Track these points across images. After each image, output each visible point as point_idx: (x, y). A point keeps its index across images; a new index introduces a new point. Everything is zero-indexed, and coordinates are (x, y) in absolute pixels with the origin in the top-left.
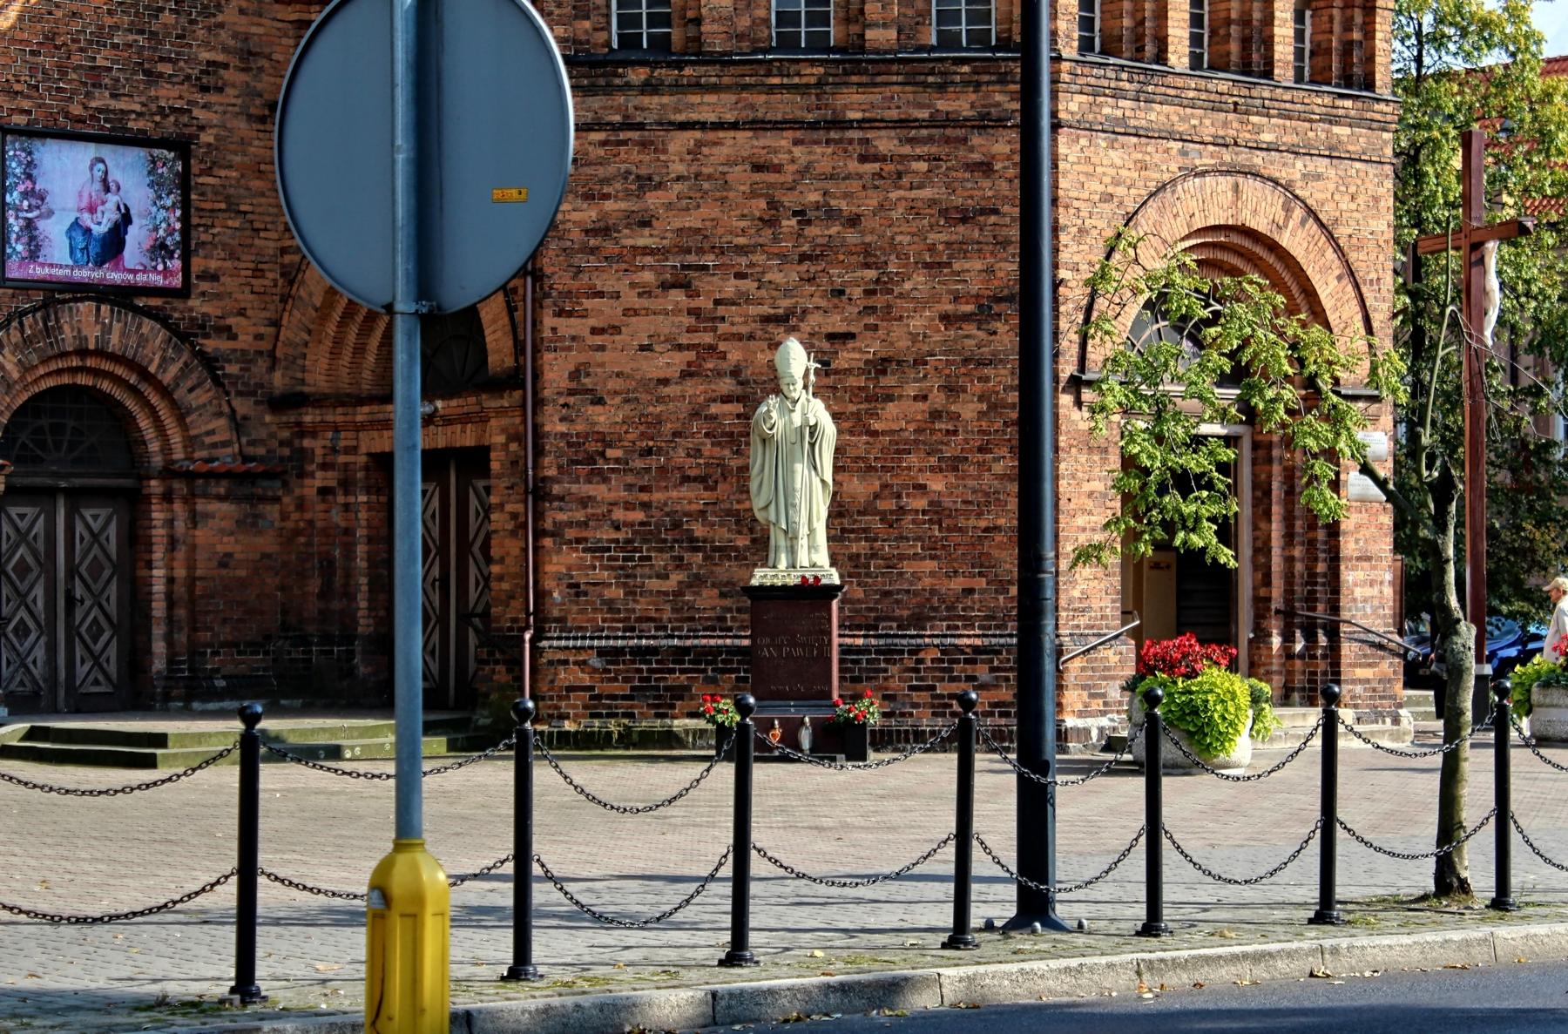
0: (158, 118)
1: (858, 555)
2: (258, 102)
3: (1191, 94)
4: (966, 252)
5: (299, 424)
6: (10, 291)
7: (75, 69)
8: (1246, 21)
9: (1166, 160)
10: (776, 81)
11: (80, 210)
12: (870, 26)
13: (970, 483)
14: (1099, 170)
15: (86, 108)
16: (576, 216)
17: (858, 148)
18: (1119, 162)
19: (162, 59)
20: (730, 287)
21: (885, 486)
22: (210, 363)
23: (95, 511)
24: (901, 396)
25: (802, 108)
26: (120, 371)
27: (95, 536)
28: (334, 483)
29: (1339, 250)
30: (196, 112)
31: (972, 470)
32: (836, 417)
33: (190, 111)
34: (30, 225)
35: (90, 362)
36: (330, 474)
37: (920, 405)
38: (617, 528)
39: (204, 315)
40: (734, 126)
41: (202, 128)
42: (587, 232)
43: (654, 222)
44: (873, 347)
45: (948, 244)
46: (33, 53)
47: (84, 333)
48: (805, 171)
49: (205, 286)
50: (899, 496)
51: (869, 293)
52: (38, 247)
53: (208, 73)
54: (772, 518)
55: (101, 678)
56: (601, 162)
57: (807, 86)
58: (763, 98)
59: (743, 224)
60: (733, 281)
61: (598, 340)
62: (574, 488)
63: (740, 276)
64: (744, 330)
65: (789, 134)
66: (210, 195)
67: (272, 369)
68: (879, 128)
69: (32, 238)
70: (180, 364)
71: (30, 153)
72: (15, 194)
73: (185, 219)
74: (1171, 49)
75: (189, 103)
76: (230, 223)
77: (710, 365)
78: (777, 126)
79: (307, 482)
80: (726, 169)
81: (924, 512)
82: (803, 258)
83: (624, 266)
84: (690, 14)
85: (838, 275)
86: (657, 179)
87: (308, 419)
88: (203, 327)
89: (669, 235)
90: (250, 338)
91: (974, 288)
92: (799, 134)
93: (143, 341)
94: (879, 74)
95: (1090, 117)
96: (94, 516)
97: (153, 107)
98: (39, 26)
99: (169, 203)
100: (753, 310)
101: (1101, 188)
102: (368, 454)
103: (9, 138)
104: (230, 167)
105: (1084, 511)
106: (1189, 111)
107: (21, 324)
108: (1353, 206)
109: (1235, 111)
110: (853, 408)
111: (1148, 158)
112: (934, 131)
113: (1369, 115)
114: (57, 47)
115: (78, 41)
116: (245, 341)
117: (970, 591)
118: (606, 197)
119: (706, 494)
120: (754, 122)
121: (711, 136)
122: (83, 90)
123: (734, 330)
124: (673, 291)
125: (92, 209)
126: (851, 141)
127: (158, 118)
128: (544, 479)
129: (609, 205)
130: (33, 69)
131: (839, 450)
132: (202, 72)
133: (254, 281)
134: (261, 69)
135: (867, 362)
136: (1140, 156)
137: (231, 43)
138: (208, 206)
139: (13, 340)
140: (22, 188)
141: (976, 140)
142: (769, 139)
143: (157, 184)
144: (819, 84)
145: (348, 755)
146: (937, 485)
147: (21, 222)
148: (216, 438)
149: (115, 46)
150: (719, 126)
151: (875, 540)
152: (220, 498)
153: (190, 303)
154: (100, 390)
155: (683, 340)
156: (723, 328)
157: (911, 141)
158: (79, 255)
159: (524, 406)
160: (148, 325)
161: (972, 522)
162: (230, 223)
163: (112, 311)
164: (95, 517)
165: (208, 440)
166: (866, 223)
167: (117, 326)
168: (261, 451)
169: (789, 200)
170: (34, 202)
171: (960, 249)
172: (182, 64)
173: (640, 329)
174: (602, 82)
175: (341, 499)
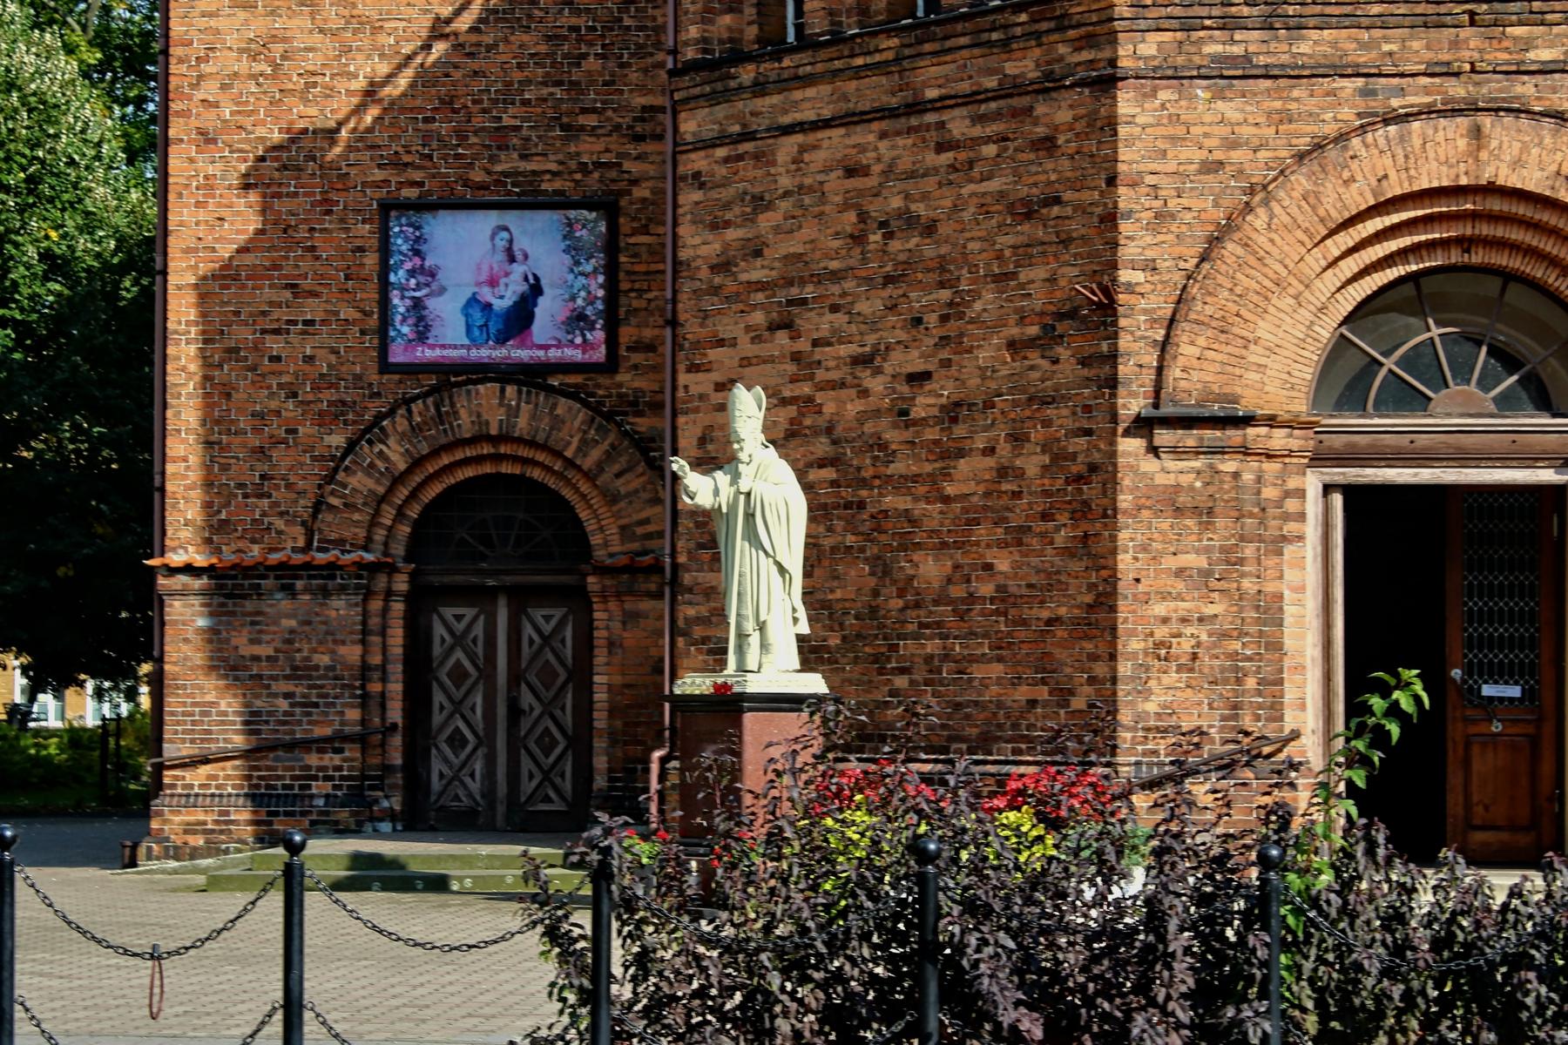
0: (578, 176)
1: (932, 657)
4: (1032, 256)
6: (397, 377)
7: (475, 133)
9: (1340, 104)
10: (859, 61)
11: (478, 284)
13: (1035, 561)
14: (1195, 130)
15: (489, 173)
16: (704, 251)
17: (933, 133)
18: (1236, 116)
19: (584, 111)
21: (957, 567)
23: (545, 612)
25: (886, 93)
27: (546, 639)
30: (627, 165)
31: (1035, 543)
33: (620, 165)
34: (417, 304)
39: (636, 390)
41: (635, 182)
43: (766, 251)
44: (944, 390)
46: (426, 120)
47: (485, 417)
49: (637, 358)
50: (968, 581)
51: (944, 319)
52: (427, 327)
53: (643, 120)
55: (552, 795)
57: (886, 62)
58: (854, 84)
59: (836, 244)
60: (829, 317)
63: (835, 309)
64: (834, 375)
65: (875, 126)
66: (644, 257)
68: (952, 107)
69: (421, 319)
70: (605, 446)
71: (418, 228)
72: (401, 273)
73: (612, 287)
75: (619, 155)
83: (741, 306)
85: (918, 300)
88: (635, 404)
89: (777, 264)
91: (1038, 305)
92: (884, 125)
93: (557, 423)
94: (946, 38)
95: (1180, 60)
96: (545, 617)
97: (573, 164)
98: (433, 91)
99: (588, 268)
100: (844, 350)
101: (1199, 155)
103: (393, 214)
105: (1165, 596)
106: (1377, 33)
107: (410, 411)
109: (1472, 23)
110: (928, 468)
111: (1293, 106)
112: (1002, 103)
114: (455, 111)
115: (480, 102)
117: (1033, 703)
121: (811, 138)
122: (486, 154)
125: (493, 282)
126: (928, 127)
127: (578, 176)
130: (426, 139)
132: (635, 119)
136: (1278, 104)
138: (642, 268)
139: (400, 429)
140: (408, 266)
143: (575, 250)
144: (898, 60)
145: (455, 887)
147: (408, 302)
151: (947, 637)
154: (531, 479)
155: (787, 393)
156: (820, 375)
158: (476, 332)
160: (563, 406)
163: (520, 392)
164: (547, 618)
165: (640, 531)
166: (944, 229)
170: (422, 279)
171: (1026, 253)
172: (610, 113)
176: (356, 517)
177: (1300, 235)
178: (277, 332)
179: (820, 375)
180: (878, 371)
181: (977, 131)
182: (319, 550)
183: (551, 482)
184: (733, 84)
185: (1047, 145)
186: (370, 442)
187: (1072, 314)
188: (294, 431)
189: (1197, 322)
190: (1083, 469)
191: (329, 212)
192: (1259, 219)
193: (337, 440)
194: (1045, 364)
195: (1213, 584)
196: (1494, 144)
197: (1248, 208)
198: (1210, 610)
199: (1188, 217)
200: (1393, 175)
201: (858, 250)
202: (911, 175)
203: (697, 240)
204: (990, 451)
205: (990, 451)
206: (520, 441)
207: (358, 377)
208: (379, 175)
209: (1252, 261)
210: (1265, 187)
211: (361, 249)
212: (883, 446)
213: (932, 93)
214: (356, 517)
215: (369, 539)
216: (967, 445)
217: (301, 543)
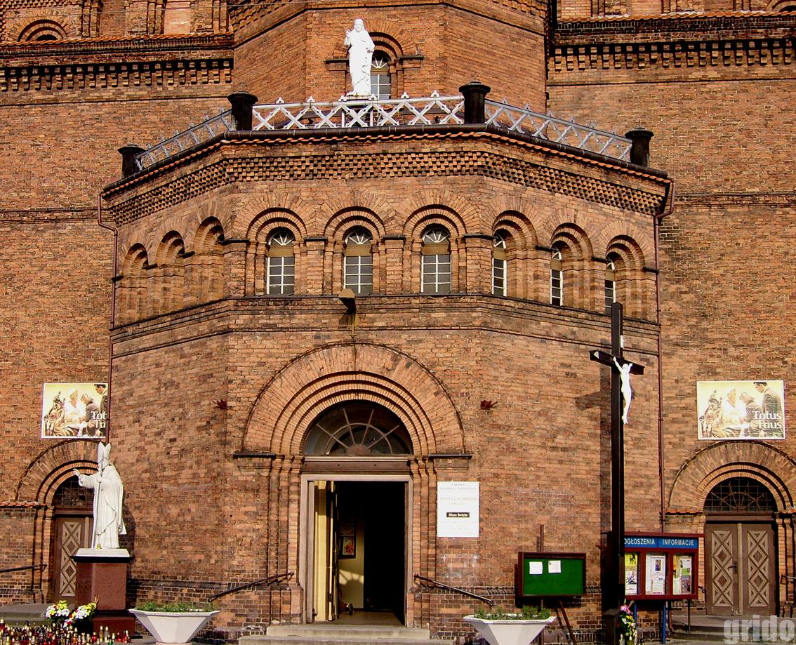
3: (320, 307)
9: (306, 342)
51: (180, 419)
59: (152, 391)
64: (151, 439)
105: (242, 521)
113: (457, 305)
166: (181, 386)
176: (33, 489)
177: (292, 389)
178: (9, 422)
179: (147, 439)
180: (162, 438)
181: (191, 351)
182: (20, 501)
184: (127, 334)
185: (209, 355)
186: (39, 462)
188: (13, 458)
189: (255, 421)
191: (28, 380)
192: (277, 383)
193: (28, 461)
194: (207, 435)
195: (259, 518)
196: (361, 356)
197: (273, 379)
198: (258, 527)
199: (252, 382)
200: (325, 367)
202: (174, 367)
204: (191, 467)
205: (191, 467)
208: (46, 367)
209: (274, 398)
210: (279, 372)
212: (162, 465)
213: (180, 338)
214: (33, 489)
215: (38, 496)
217: (14, 498)
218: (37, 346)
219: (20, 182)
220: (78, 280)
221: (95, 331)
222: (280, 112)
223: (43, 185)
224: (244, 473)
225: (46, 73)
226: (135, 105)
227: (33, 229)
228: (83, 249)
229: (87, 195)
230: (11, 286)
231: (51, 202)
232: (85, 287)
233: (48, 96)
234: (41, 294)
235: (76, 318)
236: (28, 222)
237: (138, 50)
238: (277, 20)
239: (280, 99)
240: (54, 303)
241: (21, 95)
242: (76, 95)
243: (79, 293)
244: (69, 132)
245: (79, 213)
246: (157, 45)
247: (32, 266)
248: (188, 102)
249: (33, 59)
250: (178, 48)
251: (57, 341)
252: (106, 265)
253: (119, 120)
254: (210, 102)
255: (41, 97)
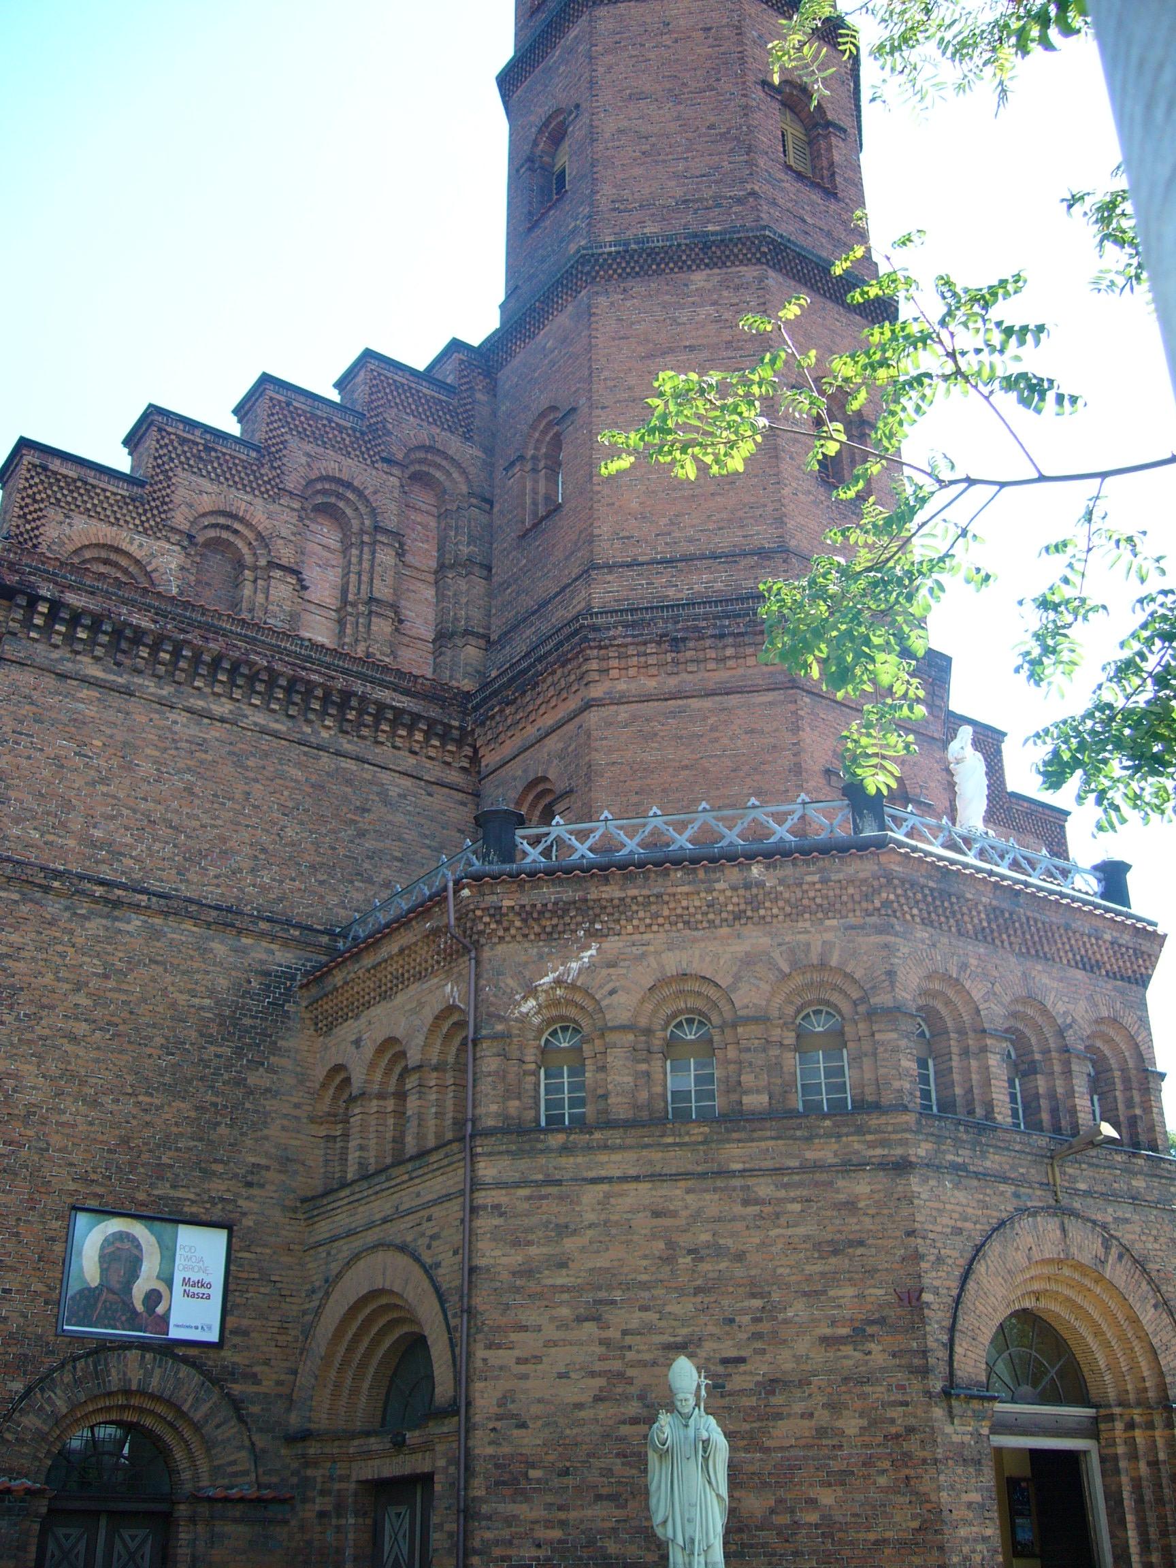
2: (292, 1196)
5: (304, 1456)
8: (1052, 1096)
10: (670, 1140)
12: (746, 1093)
16: (504, 1260)
18: (964, 1201)
19: (215, 1161)
20: (636, 1319)
21: (780, 1501)
22: (236, 1404)
23: (133, 1532)
24: (789, 1415)
26: (160, 1409)
27: (132, 1556)
28: (329, 1508)
29: (1150, 1281)
30: (240, 1202)
32: (728, 1435)
35: (134, 1401)
36: (326, 1499)
37: (806, 1423)
38: (539, 1546)
39: (234, 1363)
40: (636, 1179)
41: (244, 1214)
42: (514, 1274)
44: (760, 1368)
45: (823, 1274)
46: (110, 1151)
47: (130, 1375)
48: (696, 1216)
49: (236, 1340)
50: (792, 1512)
51: (757, 1320)
54: (670, 1534)
56: (528, 1214)
59: (645, 1263)
60: (638, 1314)
61: (522, 1369)
62: (501, 1507)
64: (647, 1357)
65: (682, 1184)
67: (289, 1410)
74: (996, 1110)
76: (262, 1290)
77: (619, 1390)
78: (675, 1177)
79: (308, 1506)
80: (630, 1216)
81: (817, 1526)
82: (698, 1291)
84: (600, 1092)
86: (572, 1227)
87: (312, 1451)
88: (233, 1374)
90: (271, 1383)
91: (847, 1313)
92: (690, 1183)
97: (206, 1197)
102: (359, 1482)
104: (265, 1246)
105: (966, 1523)
107: (74, 1368)
108: (1157, 1246)
110: (746, 1427)
116: (268, 1386)
118: (530, 1243)
119: (617, 1512)
120: (652, 1175)
121: (617, 1188)
123: (640, 1357)
124: (587, 1324)
128: (474, 1499)
129: (533, 1250)
131: (732, 1466)
133: (279, 1337)
134: (296, 1172)
135: (758, 1383)
137: (273, 1150)
138: (245, 1275)
141: (840, 1183)
142: (665, 1189)
146: (827, 1498)
148: (234, 1469)
149: (178, 1150)
150: (624, 1179)
152: (235, 1521)
153: (223, 1353)
156: (630, 1355)
157: (786, 1186)
159: (458, 1431)
160: (184, 1370)
161: (862, 1536)
162: (262, 1290)
164: (133, 1538)
165: (229, 1470)
166: (752, 1258)
167: (157, 1371)
168: (275, 1480)
169: (684, 1240)
171: (832, 1278)
173: (560, 1358)
174: (527, 1147)
175: (334, 1521)
176: (25, 1450)
181: (782, 1194)
183: (159, 1428)
186: (42, 1390)
187: (882, 1321)
190: (901, 1430)
193: (18, 1386)
201: (668, 1268)
203: (498, 1253)
206: (153, 1397)
207: (40, 1337)
208: (72, 1186)
211: (53, 1239)
214: (25, 1450)
216: (785, 1410)
218: (56, 1140)
219: (48, 813)
220: (148, 1025)
221: (174, 1129)
222: (705, 823)
223: (92, 831)
224: (960, 1429)
225: (124, 639)
226: (266, 742)
227: (67, 908)
228: (160, 969)
229: (174, 872)
230: (11, 1007)
231: (104, 867)
232: (159, 1040)
233: (112, 677)
234: (73, 1039)
235: (141, 1098)
236: (59, 894)
237: (297, 655)
238: (711, 686)
239: (655, 809)
240: (97, 1061)
241: (62, 659)
242: (164, 693)
243: (148, 1051)
244: (148, 751)
245: (162, 902)
246: (328, 659)
247: (58, 980)
248: (350, 765)
249: (110, 605)
250: (360, 676)
251: (100, 1137)
252: (202, 1008)
253: (238, 760)
254: (385, 776)
255: (100, 674)
